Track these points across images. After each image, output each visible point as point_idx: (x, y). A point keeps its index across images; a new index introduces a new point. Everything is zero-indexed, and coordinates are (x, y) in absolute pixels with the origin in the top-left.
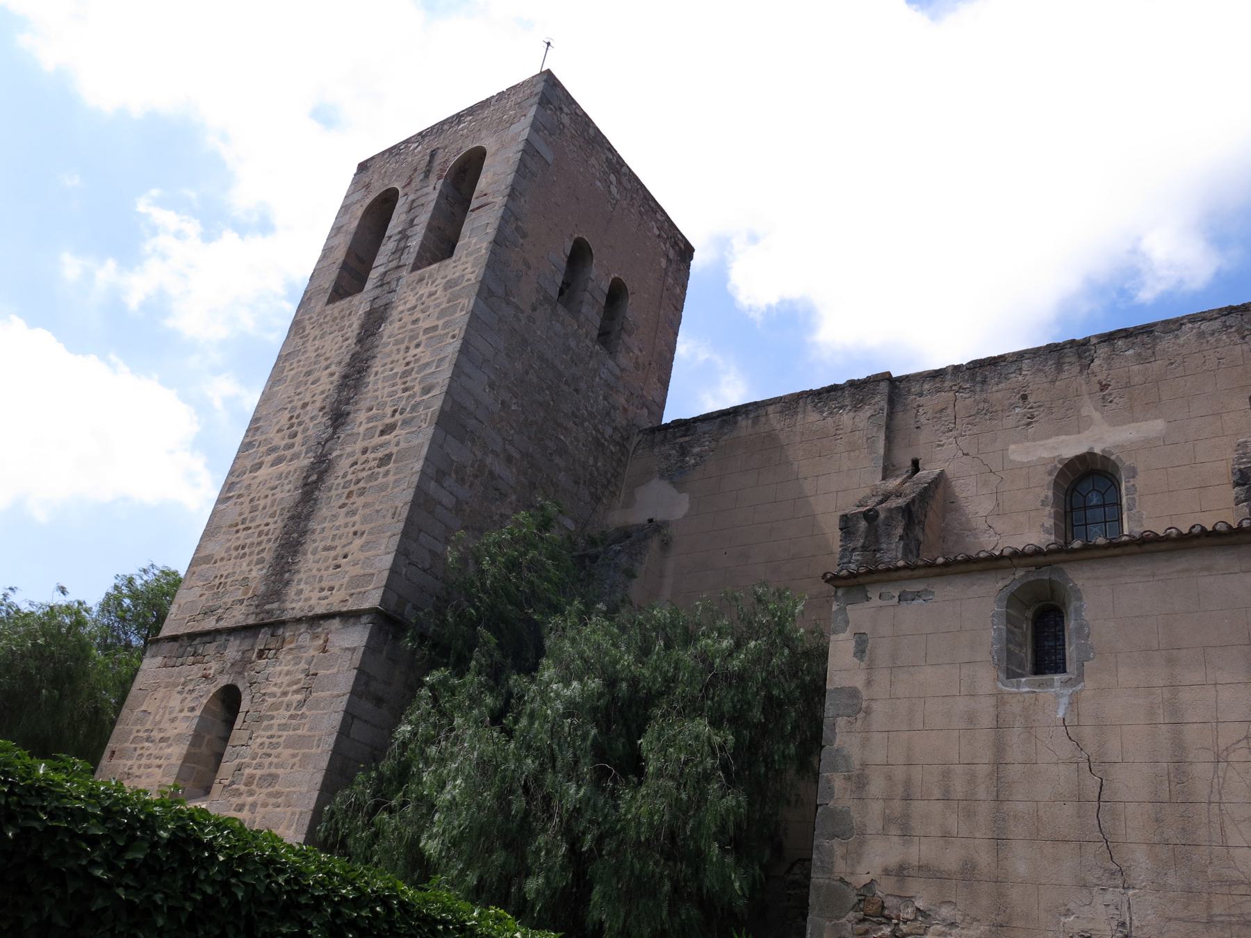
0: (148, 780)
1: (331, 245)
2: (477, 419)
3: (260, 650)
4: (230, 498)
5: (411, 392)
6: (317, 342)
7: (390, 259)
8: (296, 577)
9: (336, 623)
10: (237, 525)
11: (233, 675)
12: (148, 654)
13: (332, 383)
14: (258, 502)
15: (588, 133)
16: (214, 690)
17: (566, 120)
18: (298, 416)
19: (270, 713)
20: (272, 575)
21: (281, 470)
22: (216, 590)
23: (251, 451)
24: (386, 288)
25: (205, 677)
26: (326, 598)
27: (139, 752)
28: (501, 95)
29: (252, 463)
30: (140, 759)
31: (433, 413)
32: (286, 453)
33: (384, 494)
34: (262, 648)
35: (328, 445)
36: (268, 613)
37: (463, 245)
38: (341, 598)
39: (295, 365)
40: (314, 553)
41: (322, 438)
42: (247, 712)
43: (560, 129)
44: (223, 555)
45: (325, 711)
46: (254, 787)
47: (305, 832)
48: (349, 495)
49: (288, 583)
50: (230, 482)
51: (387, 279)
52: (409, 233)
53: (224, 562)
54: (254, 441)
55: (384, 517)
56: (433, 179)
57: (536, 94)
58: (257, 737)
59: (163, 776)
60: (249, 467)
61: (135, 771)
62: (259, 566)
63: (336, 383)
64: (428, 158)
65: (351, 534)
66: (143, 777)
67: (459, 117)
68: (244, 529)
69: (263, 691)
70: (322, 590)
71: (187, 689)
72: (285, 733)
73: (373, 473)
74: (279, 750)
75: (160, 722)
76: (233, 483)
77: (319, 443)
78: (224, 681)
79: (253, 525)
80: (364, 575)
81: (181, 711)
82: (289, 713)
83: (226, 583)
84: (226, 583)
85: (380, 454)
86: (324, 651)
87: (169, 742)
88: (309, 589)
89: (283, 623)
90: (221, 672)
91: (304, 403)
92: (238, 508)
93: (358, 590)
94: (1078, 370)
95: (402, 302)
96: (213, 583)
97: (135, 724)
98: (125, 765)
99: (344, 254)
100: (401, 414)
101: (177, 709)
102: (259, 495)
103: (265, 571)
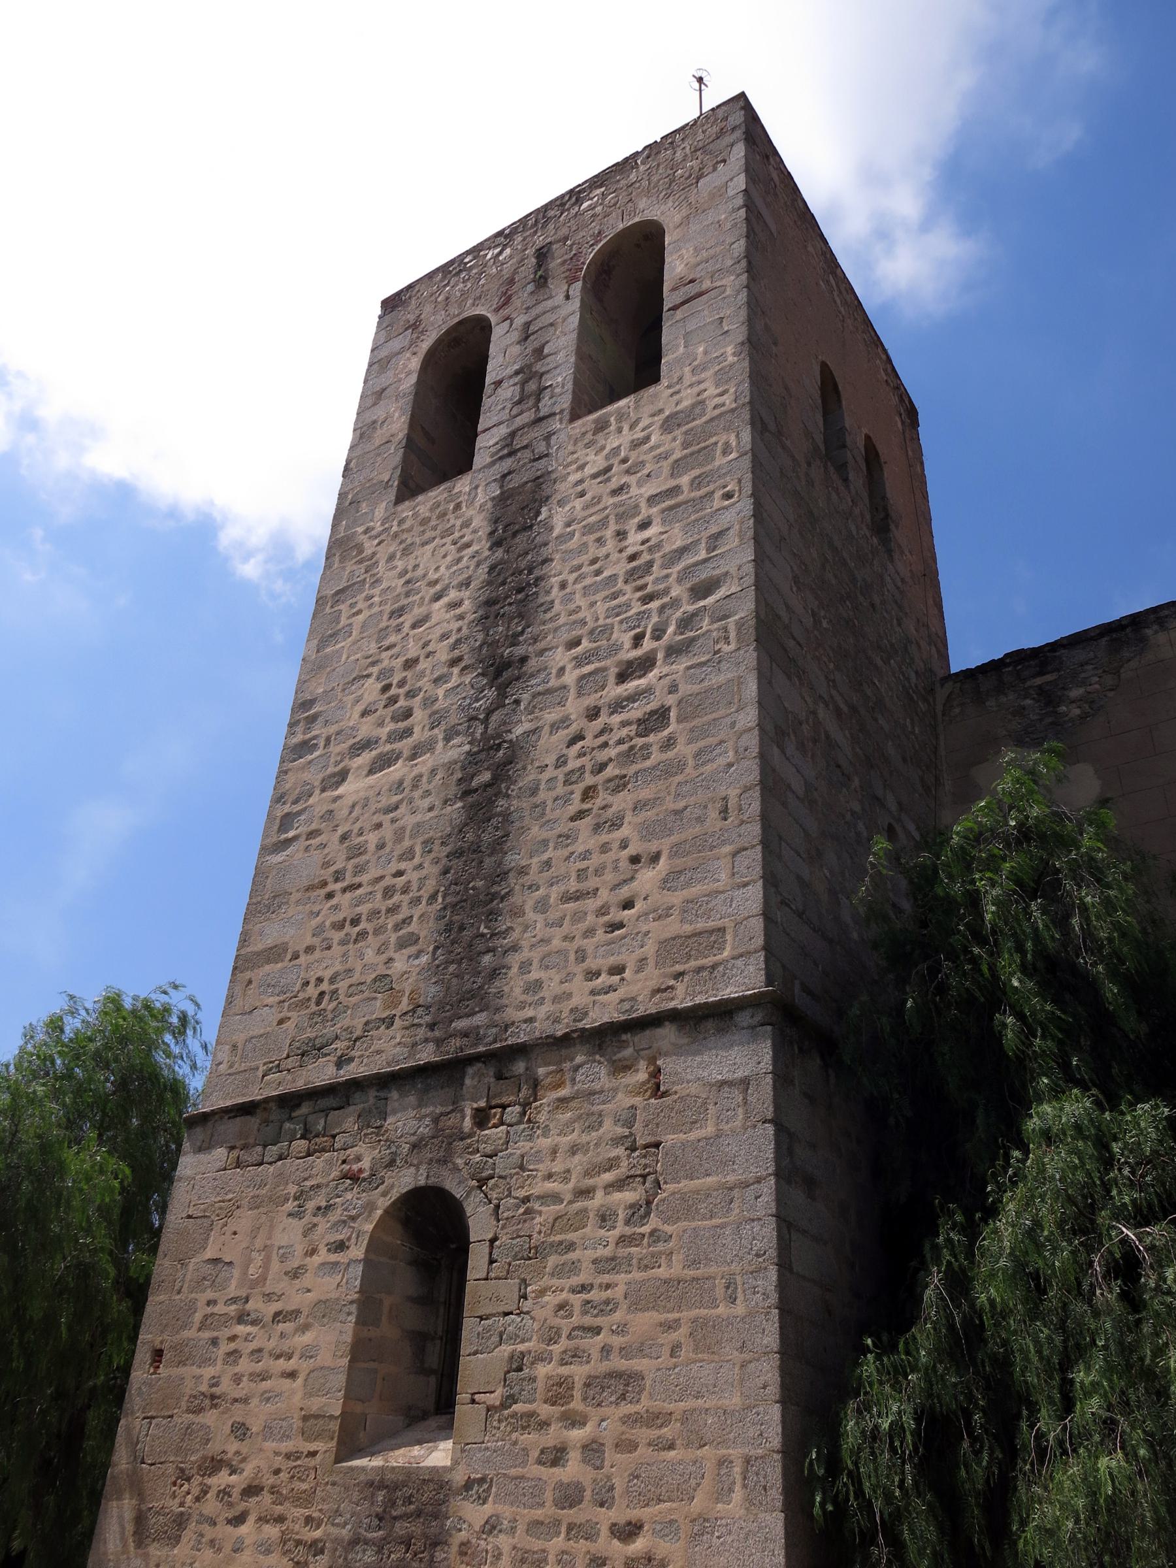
0: (269, 1407)
1: (369, 421)
2: (795, 639)
3: (478, 1110)
4: (288, 842)
5: (666, 600)
6: (400, 564)
7: (514, 412)
8: (515, 960)
9: (667, 1034)
10: (324, 884)
11: (423, 1167)
12: (186, 1146)
13: (461, 617)
14: (361, 839)
16: (383, 1203)
18: (402, 684)
19: (558, 1238)
20: (448, 963)
21: (397, 776)
22: (314, 1008)
23: (310, 757)
25: (354, 1178)
26: (611, 989)
27: (225, 1347)
28: (652, 149)
29: (320, 776)
30: (236, 1362)
31: (740, 625)
32: (397, 746)
33: (679, 778)
34: (482, 1104)
35: (495, 717)
36: (466, 1035)
38: (653, 984)
39: (360, 606)
40: (542, 906)
41: (478, 709)
42: (493, 1241)
44: (309, 940)
45: (716, 1221)
46: (577, 1404)
47: (779, 1504)
48: (589, 793)
49: (495, 973)
50: (279, 814)
52: (539, 367)
53: (317, 954)
54: (315, 738)
55: (700, 820)
56: (558, 288)
57: (733, 129)
58: (542, 1292)
59: (309, 1395)
60: (317, 784)
61: (226, 1386)
62: (407, 952)
63: (470, 617)
64: (534, 260)
65: (624, 864)
66: (255, 1402)
67: (575, 195)
68: (344, 890)
69: (522, 1193)
70: (593, 975)
71: (311, 1205)
72: (621, 1278)
73: (632, 748)
74: (618, 1316)
75: (263, 1279)
76: (288, 814)
77: (473, 718)
78: (405, 1180)
79: (364, 878)
80: (694, 935)
81: (313, 1252)
82: (616, 1233)
83: (335, 991)
84: (335, 991)
85: (636, 711)
86: (657, 1092)
87: (302, 1320)
88: (557, 978)
89: (521, 1050)
90: (391, 1164)
91: (407, 661)
92: (317, 857)
93: (693, 964)
96: (301, 996)
97: (199, 1283)
98: (198, 1378)
99: (406, 426)
100: (657, 638)
101: (299, 1249)
102: (358, 825)
103: (424, 959)
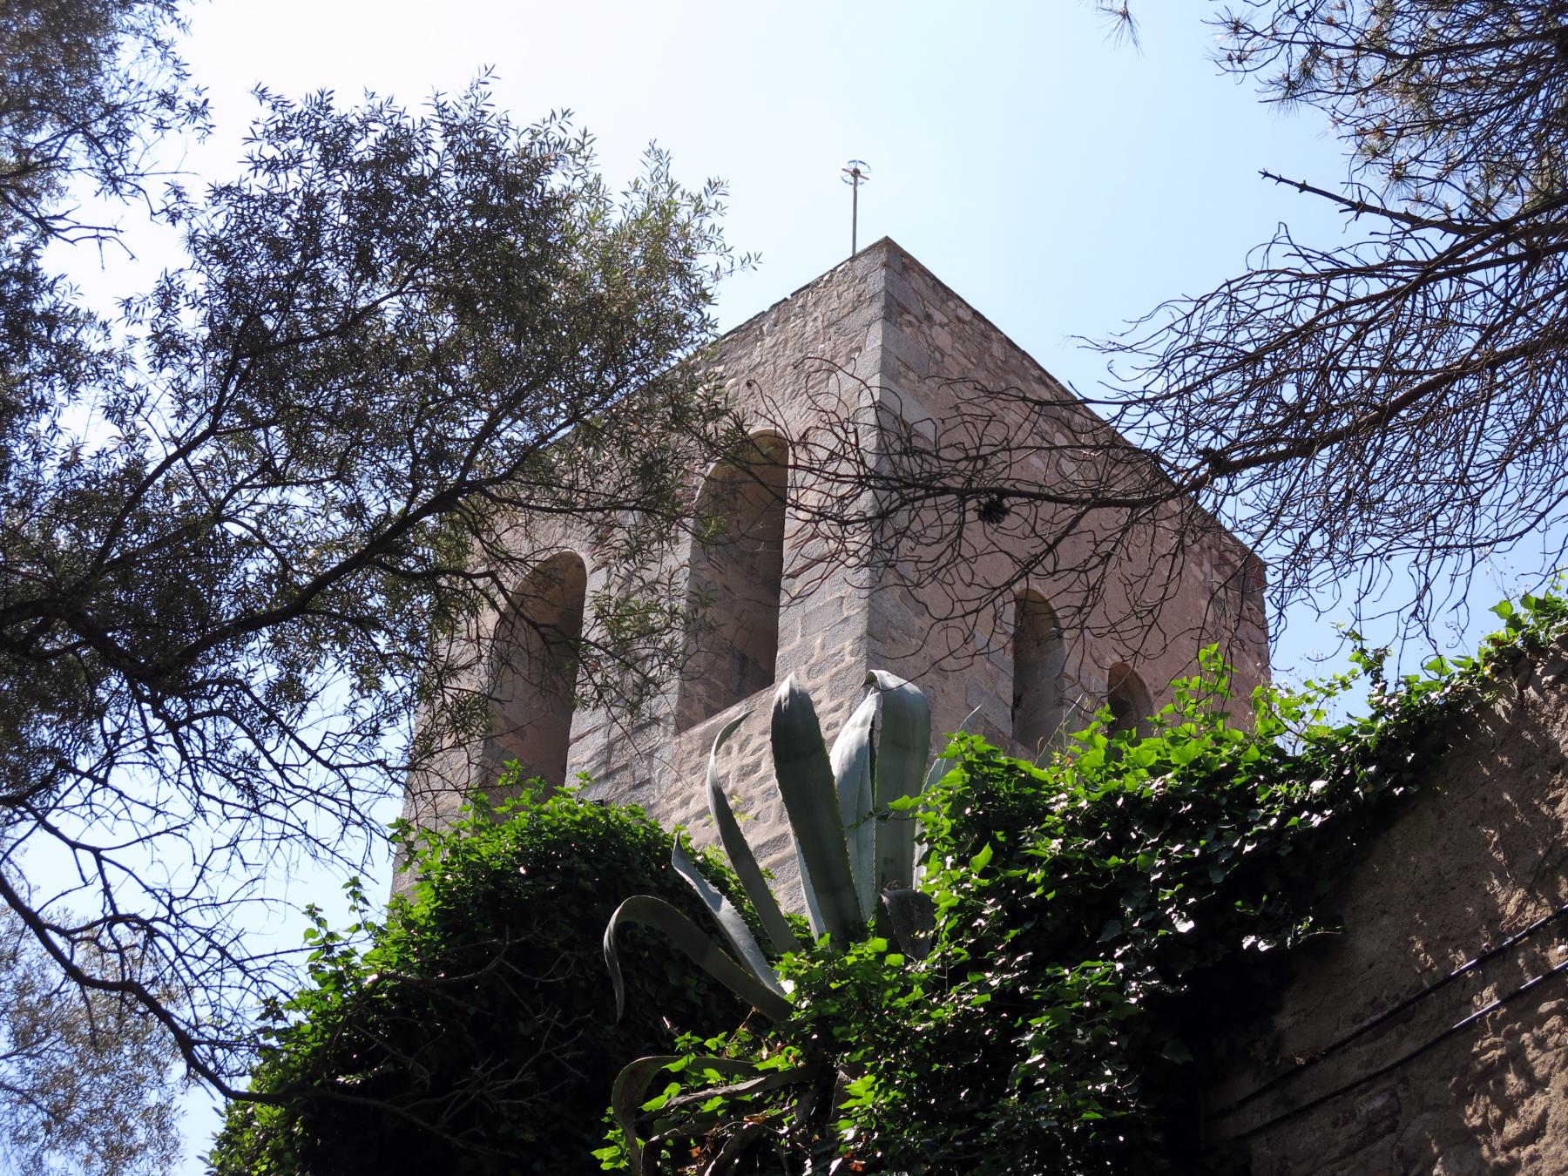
15: (991, 355)
17: (943, 338)
24: (625, 778)
37: (794, 653)
43: (937, 363)
51: (617, 761)
94: (82, 451)
95: (678, 800)
